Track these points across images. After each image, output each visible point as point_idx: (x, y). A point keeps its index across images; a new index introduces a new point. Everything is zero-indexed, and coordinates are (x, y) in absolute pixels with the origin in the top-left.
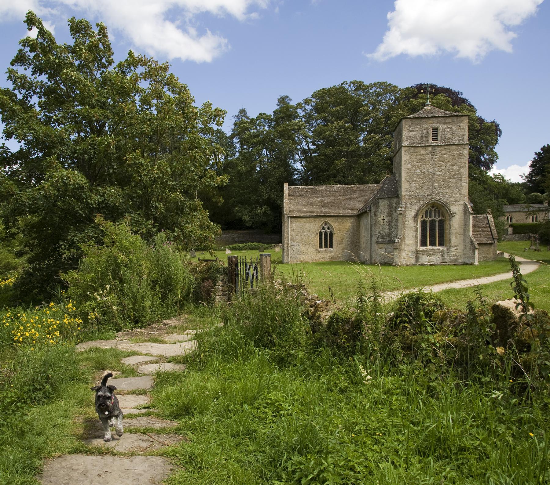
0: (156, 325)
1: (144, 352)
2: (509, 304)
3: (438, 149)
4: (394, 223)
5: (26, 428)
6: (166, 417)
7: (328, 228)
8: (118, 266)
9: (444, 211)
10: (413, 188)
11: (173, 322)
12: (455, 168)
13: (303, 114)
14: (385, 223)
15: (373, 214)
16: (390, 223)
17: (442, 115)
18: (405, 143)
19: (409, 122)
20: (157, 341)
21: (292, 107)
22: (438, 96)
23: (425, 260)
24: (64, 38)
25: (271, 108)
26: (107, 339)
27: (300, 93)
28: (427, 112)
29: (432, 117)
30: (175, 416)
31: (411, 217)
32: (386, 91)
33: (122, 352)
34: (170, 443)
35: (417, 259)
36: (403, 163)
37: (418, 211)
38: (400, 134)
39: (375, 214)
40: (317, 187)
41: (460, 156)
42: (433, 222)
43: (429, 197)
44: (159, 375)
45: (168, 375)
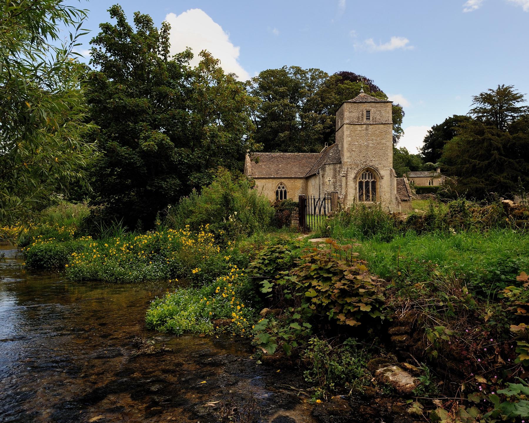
3: (370, 127)
4: (338, 184)
7: (283, 188)
12: (384, 141)
13: (251, 90)
14: (331, 183)
15: (321, 176)
16: (335, 183)
17: (373, 101)
18: (346, 121)
19: (349, 105)
28: (362, 98)
29: (366, 102)
31: (351, 179)
36: (345, 137)
37: (357, 173)
38: (342, 114)
39: (323, 177)
43: (365, 163)
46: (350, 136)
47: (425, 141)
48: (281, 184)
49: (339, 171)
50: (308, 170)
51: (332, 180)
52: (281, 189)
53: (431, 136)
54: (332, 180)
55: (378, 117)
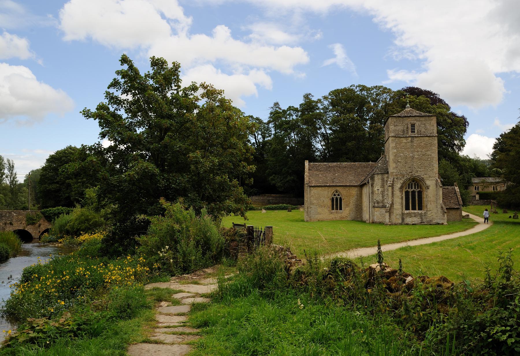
0: (198, 273)
1: (187, 291)
2: (375, 266)
3: (416, 139)
4: (386, 193)
5: (118, 330)
6: (194, 327)
7: (339, 195)
8: (174, 231)
9: (422, 184)
10: (399, 167)
11: (209, 271)
12: (429, 153)
13: (321, 107)
14: (379, 192)
16: (383, 192)
17: (418, 115)
19: (395, 119)
20: (196, 283)
21: (314, 101)
22: (420, 97)
23: (408, 220)
24: (144, 69)
25: (297, 102)
26: (165, 282)
27: (320, 92)
28: (407, 113)
30: (199, 327)
31: (397, 188)
32: (384, 92)
33: (173, 290)
34: (196, 339)
35: (403, 219)
36: (390, 149)
39: (372, 186)
40: (330, 164)
41: (431, 145)
42: (413, 192)
43: (410, 174)
44: (193, 304)
45: (199, 304)
46: (396, 147)
47: (495, 148)
48: (337, 192)
49: (387, 181)
50: (363, 178)
51: (380, 190)
52: (337, 196)
53: (500, 143)
54: (380, 190)
55: (423, 130)
